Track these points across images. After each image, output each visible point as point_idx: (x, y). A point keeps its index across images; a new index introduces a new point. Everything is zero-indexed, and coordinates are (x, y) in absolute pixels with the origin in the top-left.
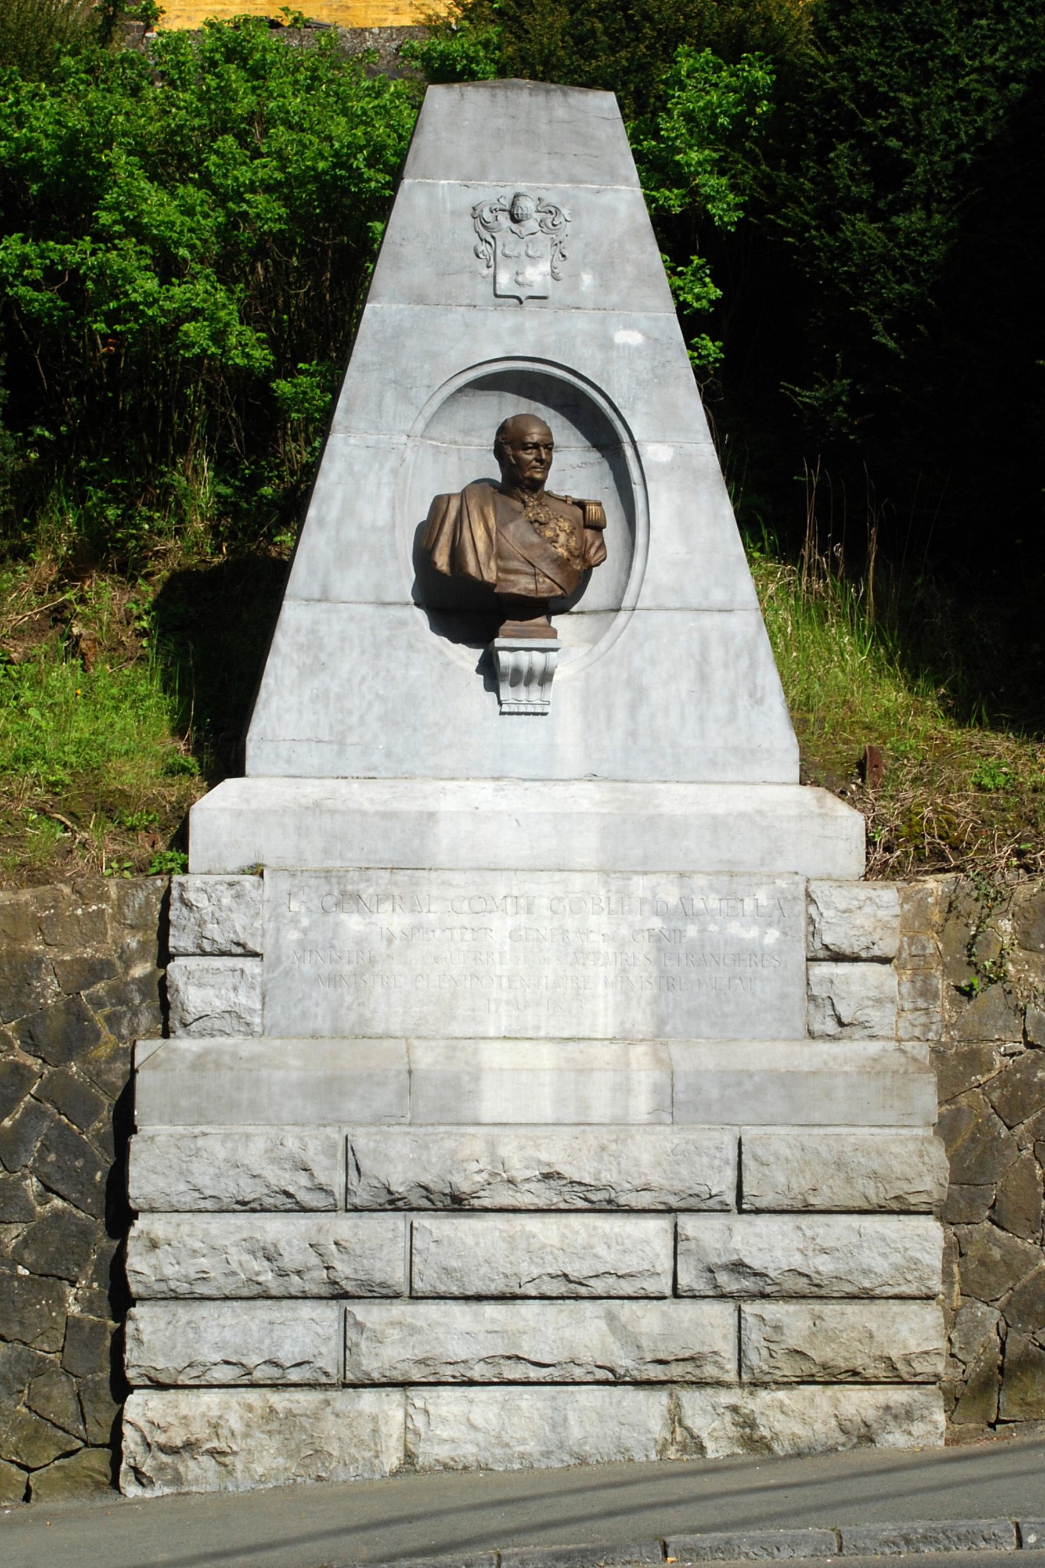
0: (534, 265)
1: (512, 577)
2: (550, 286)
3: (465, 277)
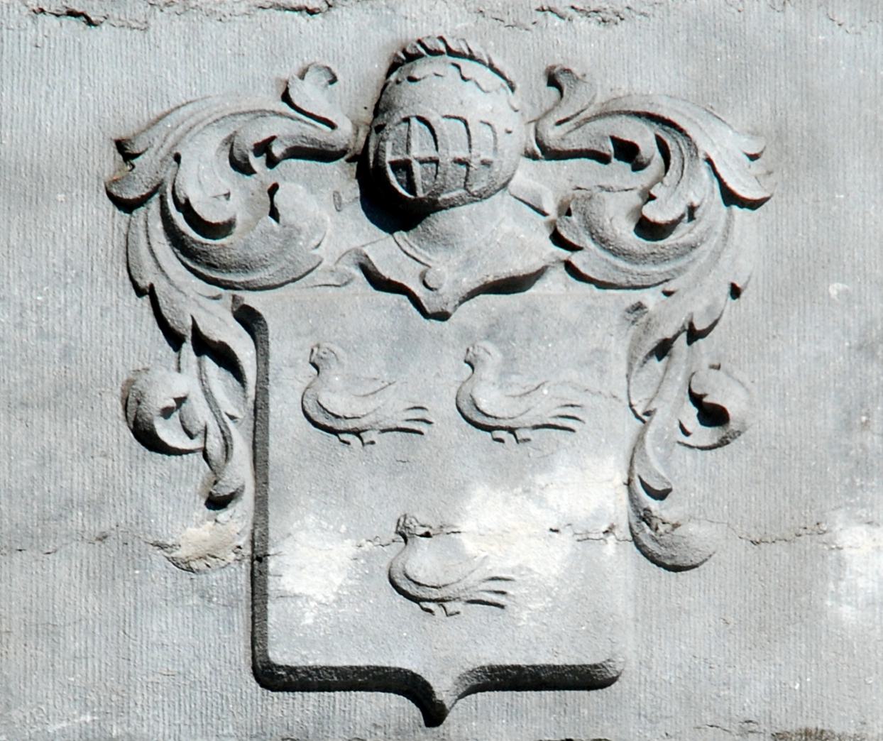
0: (510, 478)
2: (621, 603)
3: (63, 579)
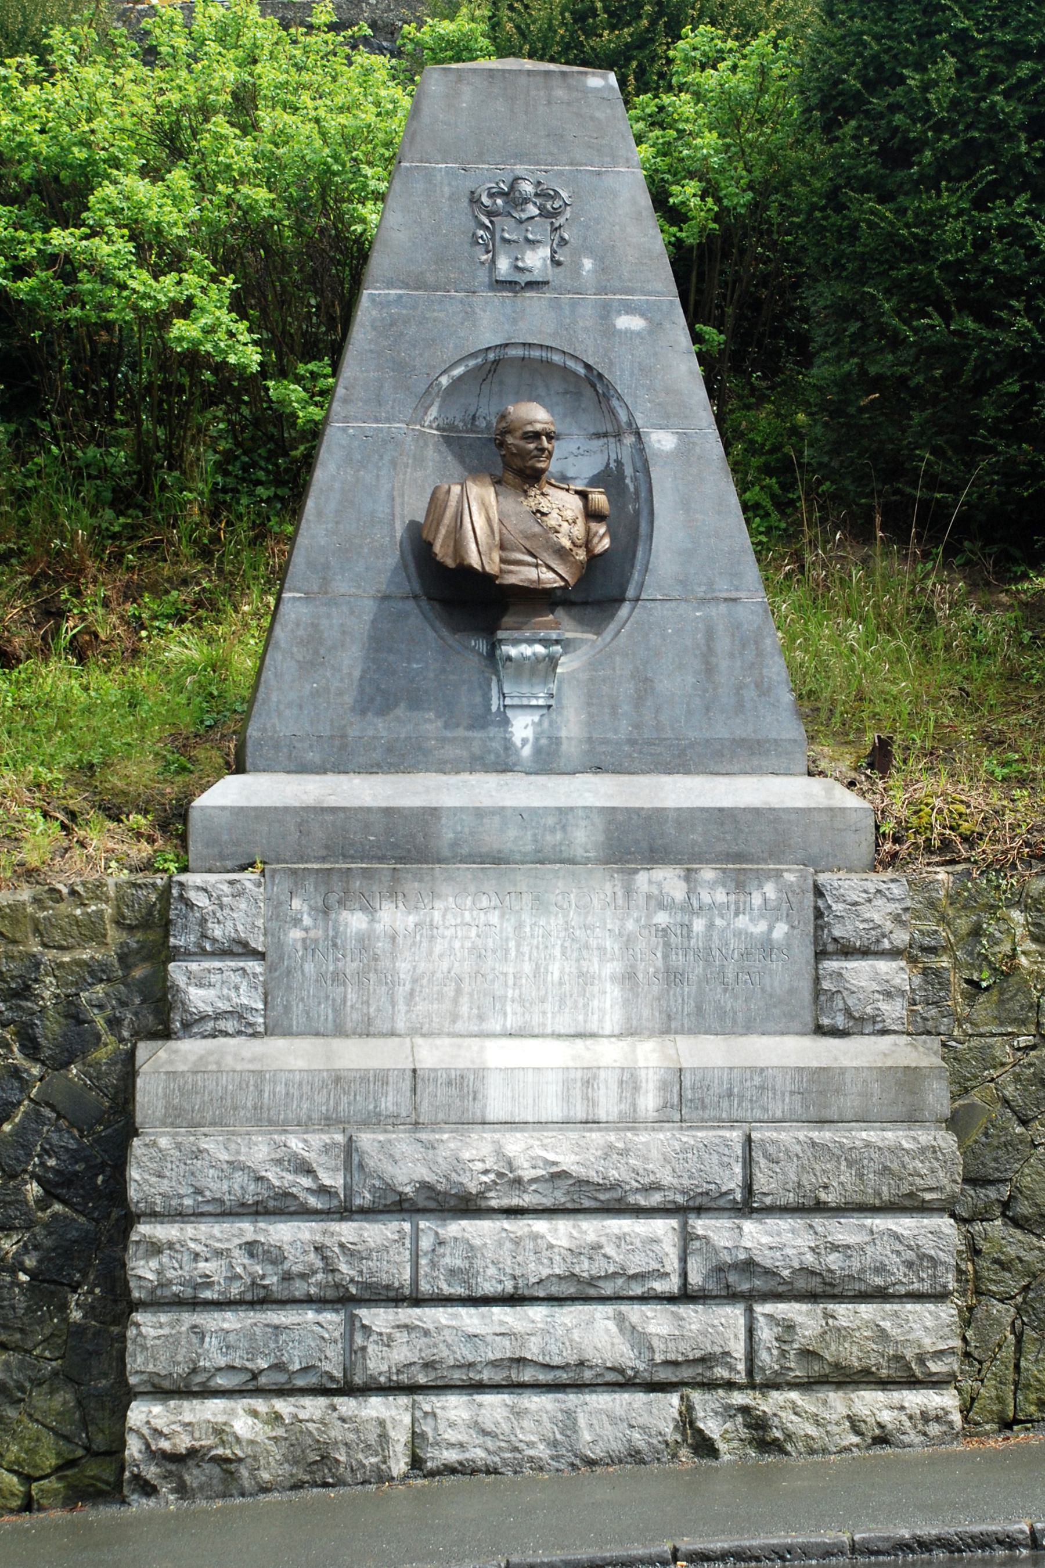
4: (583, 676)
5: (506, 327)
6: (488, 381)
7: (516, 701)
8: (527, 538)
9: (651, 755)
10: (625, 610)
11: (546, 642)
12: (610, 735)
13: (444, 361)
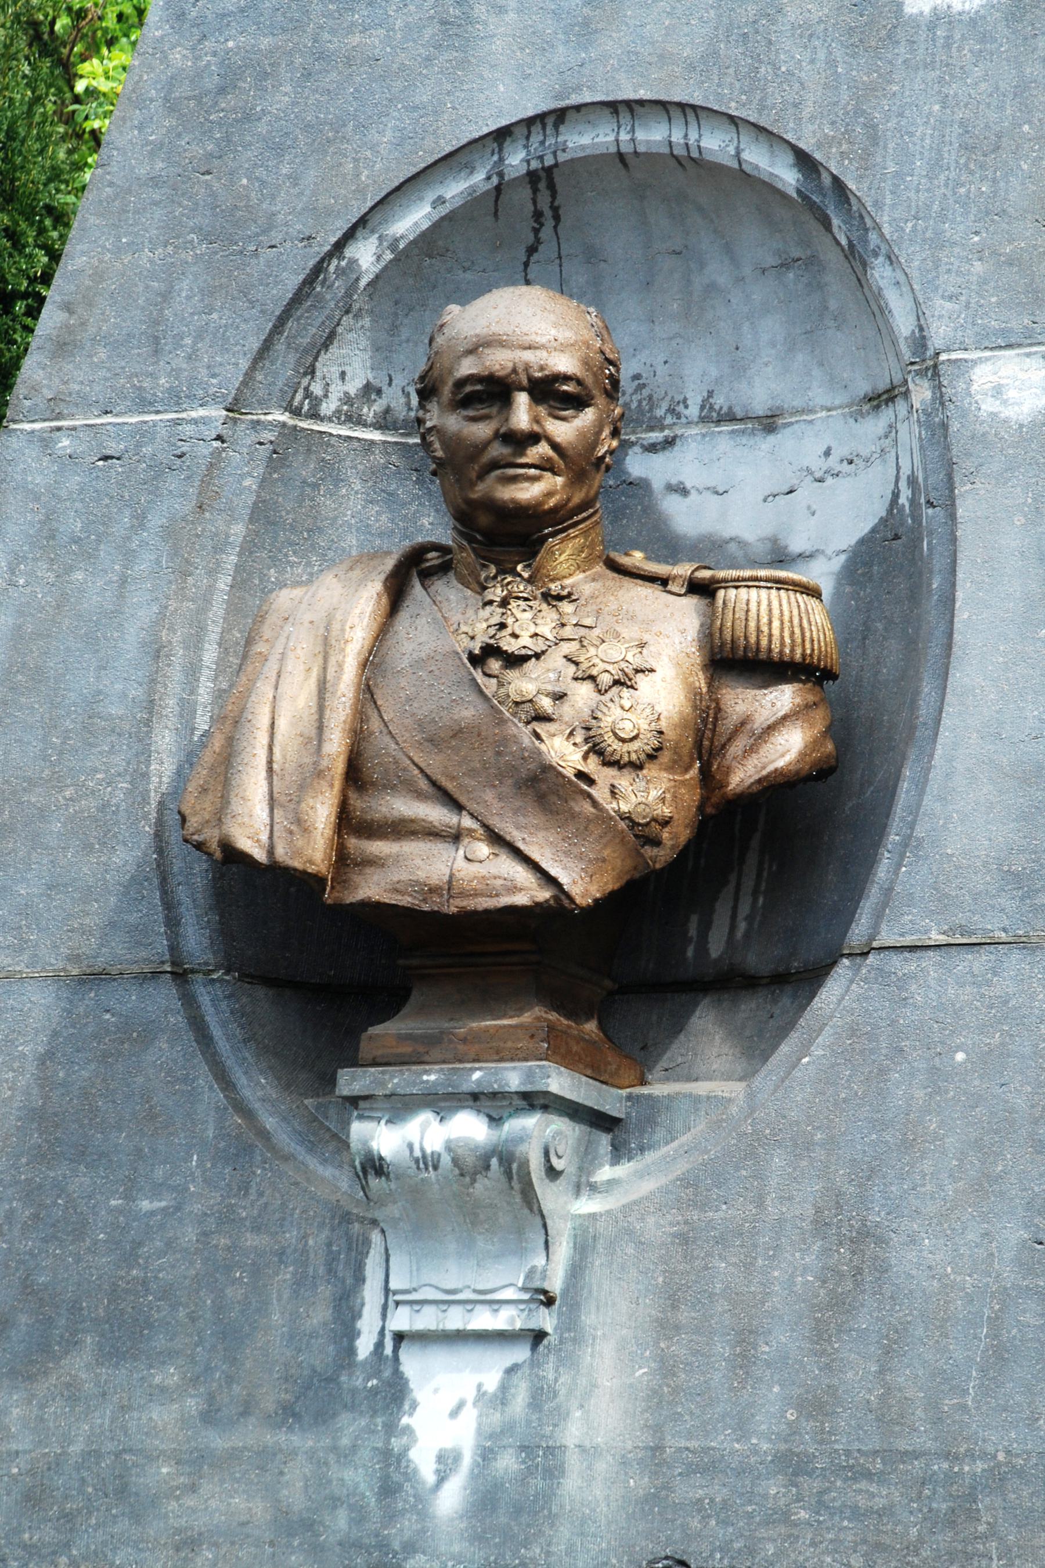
1: (378, 847)
4: (656, 1228)
5: (561, 54)
6: (548, 250)
7: (427, 1320)
8: (433, 741)
9: (856, 1514)
10: (837, 993)
11: (490, 1103)
12: (723, 1441)
13: (361, 191)
